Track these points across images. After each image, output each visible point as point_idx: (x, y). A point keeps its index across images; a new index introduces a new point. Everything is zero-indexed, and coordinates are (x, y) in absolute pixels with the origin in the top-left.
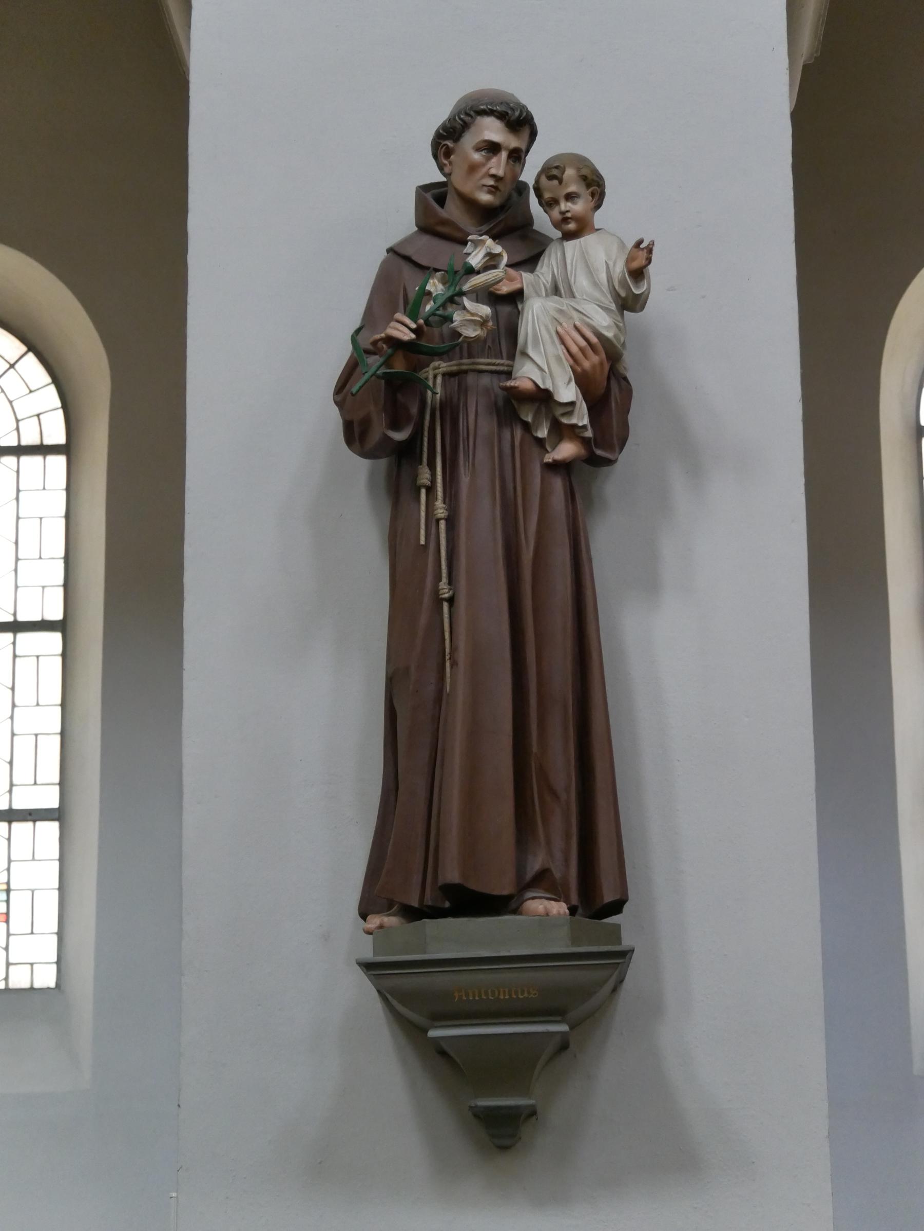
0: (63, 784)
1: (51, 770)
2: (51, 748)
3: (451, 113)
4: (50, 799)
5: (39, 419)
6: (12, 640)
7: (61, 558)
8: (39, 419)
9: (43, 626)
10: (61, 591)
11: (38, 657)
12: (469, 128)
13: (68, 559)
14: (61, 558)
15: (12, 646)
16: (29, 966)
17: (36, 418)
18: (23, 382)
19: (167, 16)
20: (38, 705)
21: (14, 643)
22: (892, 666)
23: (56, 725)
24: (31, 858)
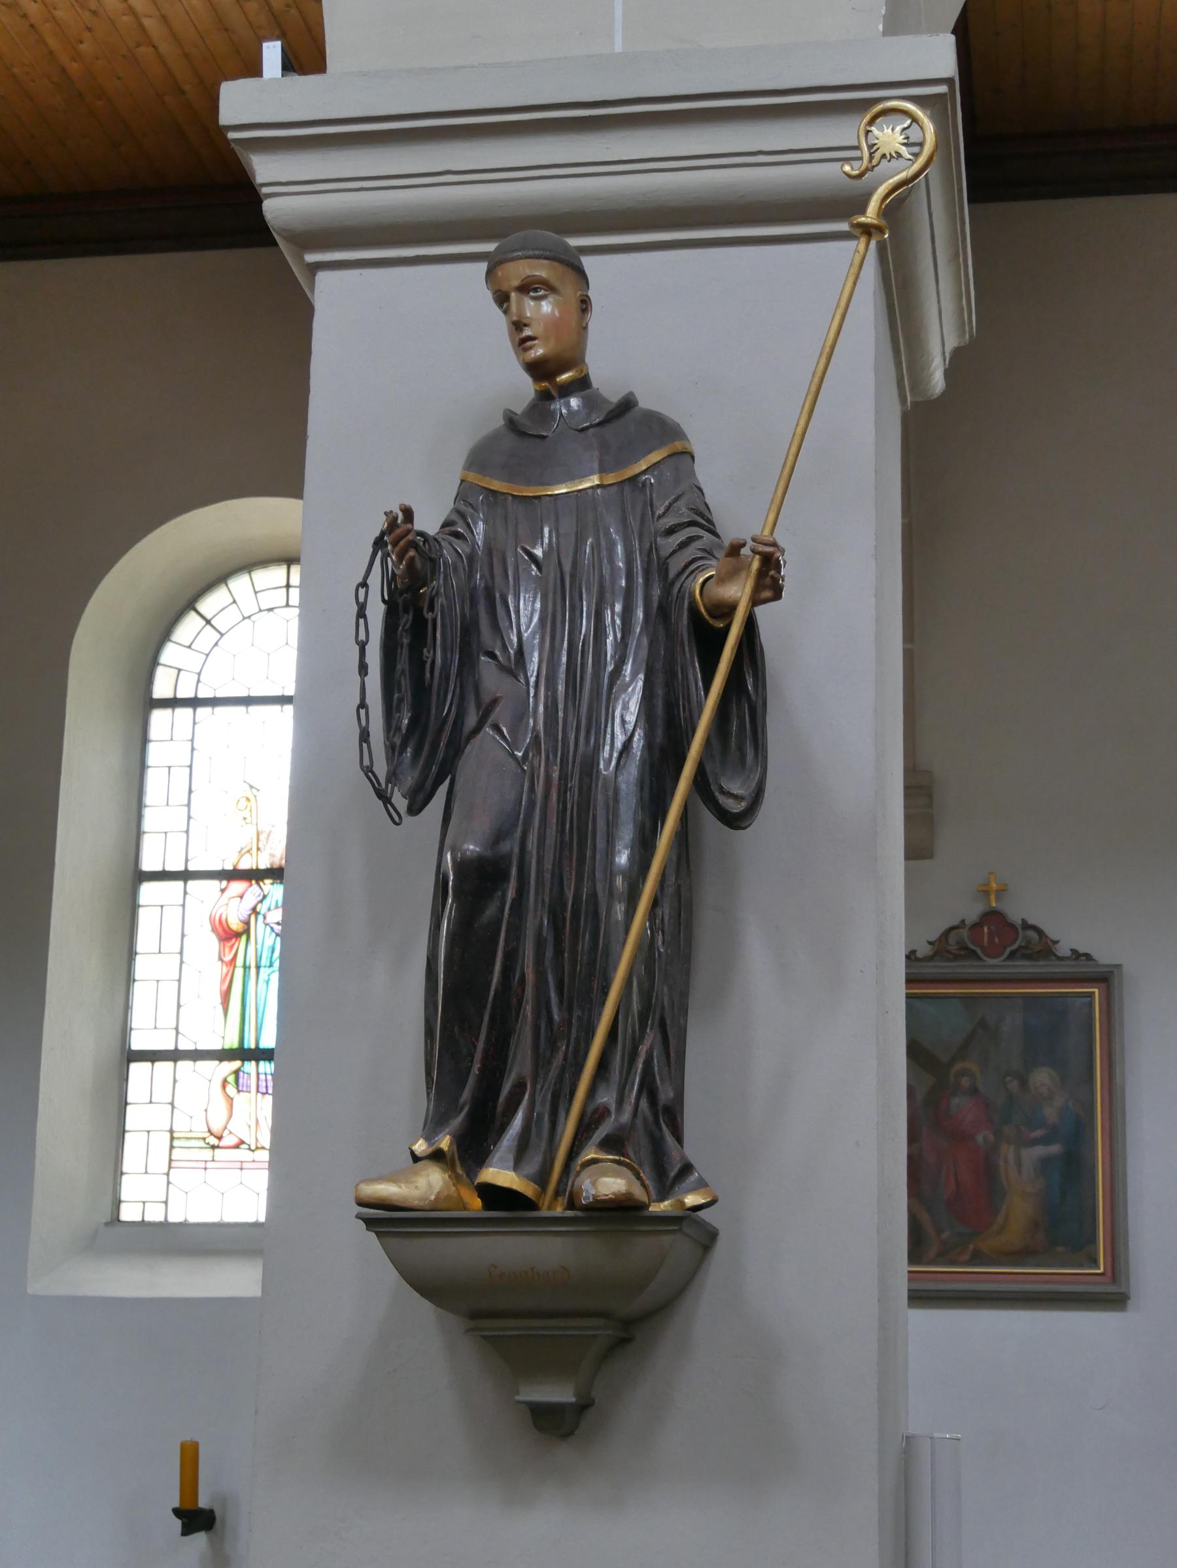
0: (133, 907)
1: (146, 920)
2: (145, 939)
3: (667, 416)
4: (148, 891)
5: (192, 644)
6: (189, 863)
7: (129, 1131)
8: (192, 644)
9: (152, 1056)
10: (126, 1167)
11: (146, 1173)
12: (676, 832)
13: (143, 767)
14: (129, 1131)
15: (181, 1003)
16: (142, 1204)
17: (193, 647)
18: (218, 628)
19: (626, 1091)
20: (162, 906)
21: (187, 861)
22: (956, 19)
23: (152, 748)
24: (158, 952)
